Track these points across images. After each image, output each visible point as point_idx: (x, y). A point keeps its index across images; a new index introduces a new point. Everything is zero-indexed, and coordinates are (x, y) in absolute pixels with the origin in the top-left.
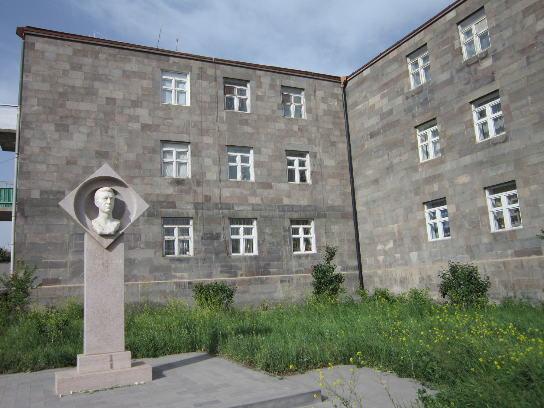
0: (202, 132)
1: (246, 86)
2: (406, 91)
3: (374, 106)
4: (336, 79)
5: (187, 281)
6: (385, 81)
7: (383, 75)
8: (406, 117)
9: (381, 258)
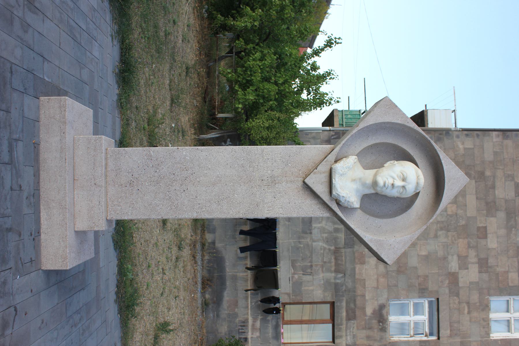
5: (249, 336)
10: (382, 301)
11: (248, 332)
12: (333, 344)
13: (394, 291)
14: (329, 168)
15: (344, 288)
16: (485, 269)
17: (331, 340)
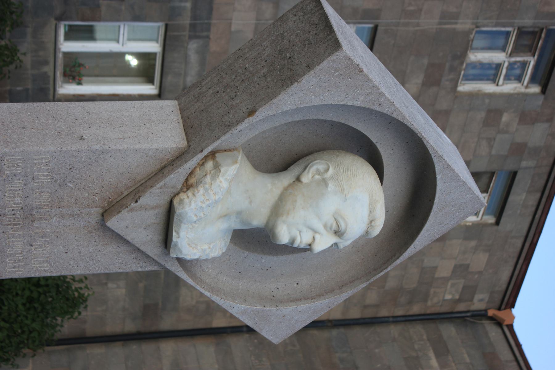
1: (533, 80)
14: (167, 198)
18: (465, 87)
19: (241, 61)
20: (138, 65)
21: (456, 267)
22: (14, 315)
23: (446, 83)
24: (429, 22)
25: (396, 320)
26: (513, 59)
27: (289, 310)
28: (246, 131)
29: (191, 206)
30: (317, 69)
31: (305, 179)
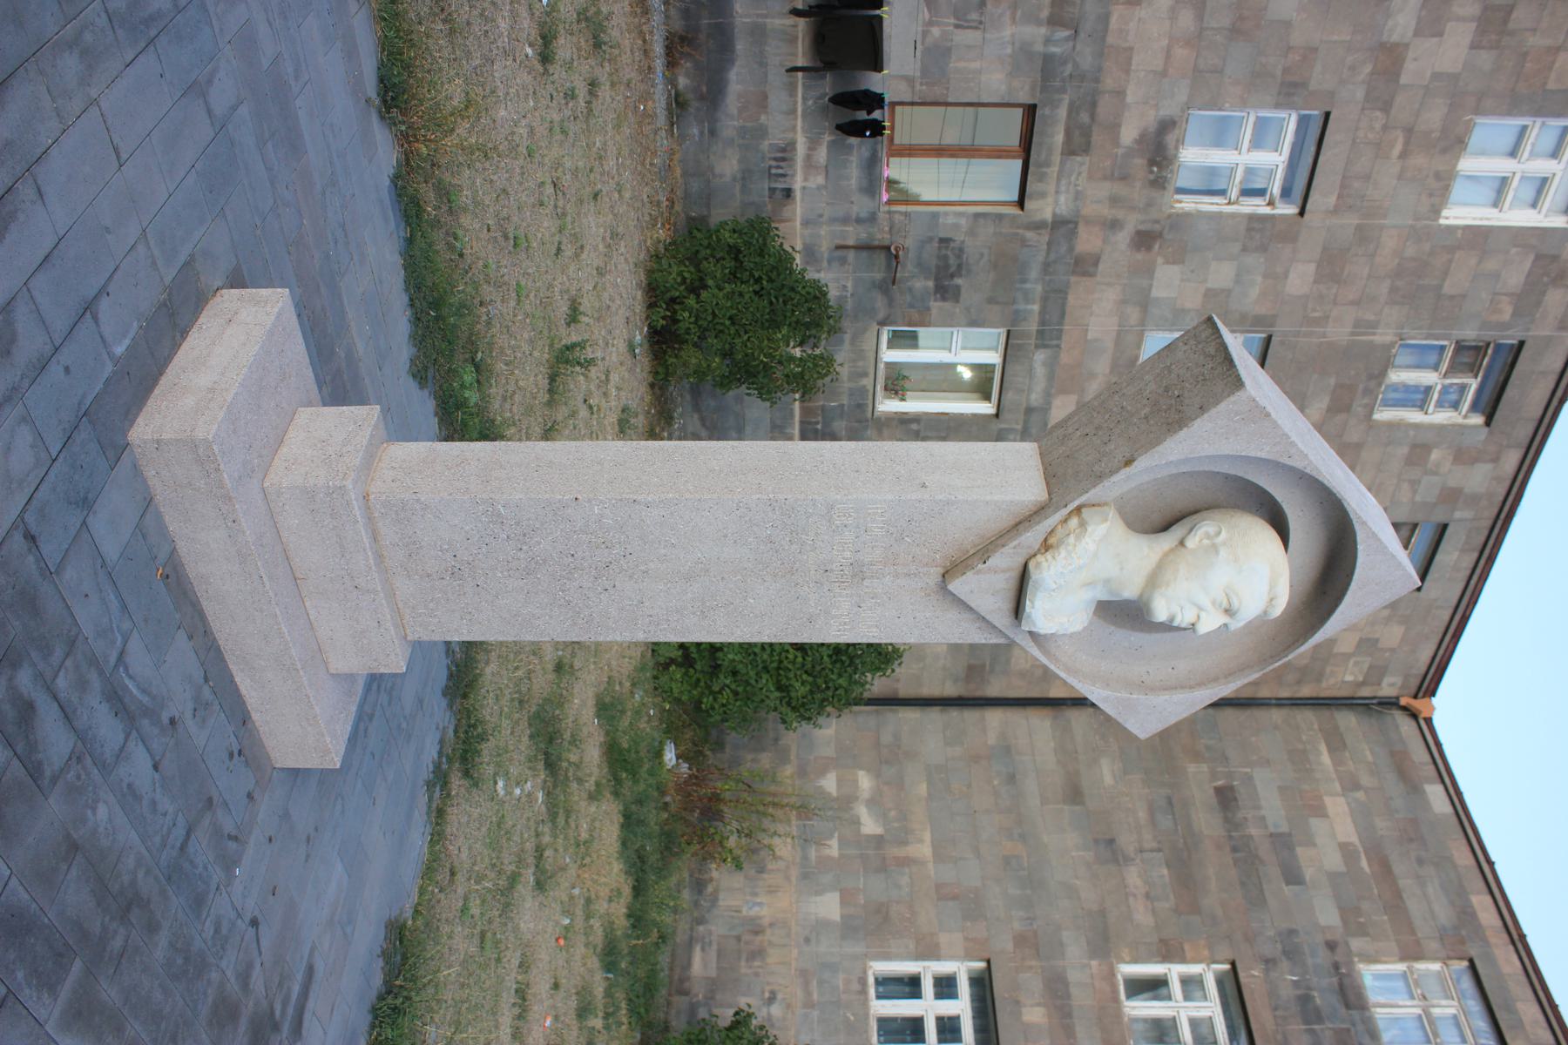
0: (1331, 266)
1: (1474, 407)
2: (1356, 944)
3: (1321, 812)
4: (1429, 683)
5: (798, 184)
6: (1399, 868)
7: (1420, 861)
8: (1271, 933)
9: (830, 783)
10: (1169, 109)
11: (793, 176)
12: (1015, 211)
13: (1207, 87)
14: (1021, 560)
15: (1069, 68)
16: (1493, 37)
17: (1016, 198)
18: (1383, 415)
19: (1116, 397)
20: (972, 378)
21: (1361, 641)
22: (818, 668)
23: (1358, 408)
24: (1339, 332)
25: (1280, 703)
26: (1448, 381)
27: (1162, 699)
28: (1121, 483)
29: (1048, 572)
30: (1213, 411)
31: (1191, 543)
